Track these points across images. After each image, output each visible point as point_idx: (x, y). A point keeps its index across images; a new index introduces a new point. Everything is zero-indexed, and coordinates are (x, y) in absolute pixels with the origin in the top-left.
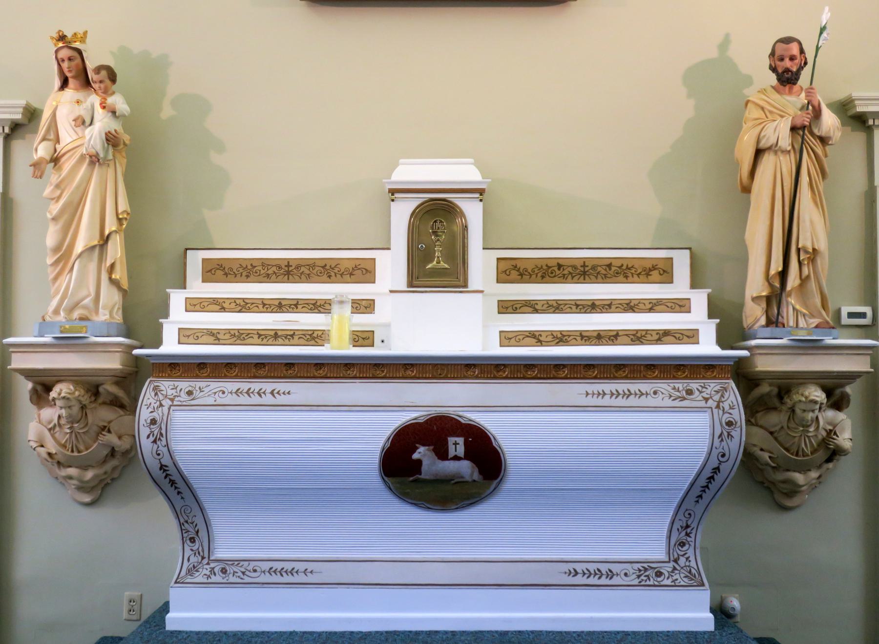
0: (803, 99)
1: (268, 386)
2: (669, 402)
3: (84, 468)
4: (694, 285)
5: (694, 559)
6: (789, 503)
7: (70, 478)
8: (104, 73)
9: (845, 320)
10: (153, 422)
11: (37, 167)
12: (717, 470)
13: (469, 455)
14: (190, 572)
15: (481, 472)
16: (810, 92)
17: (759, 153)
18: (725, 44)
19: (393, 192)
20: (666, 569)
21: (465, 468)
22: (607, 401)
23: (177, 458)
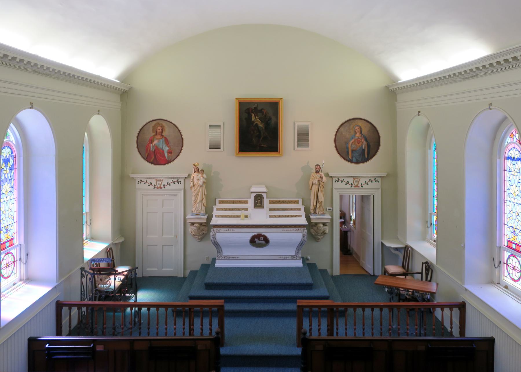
1: (231, 229)
2: (295, 232)
6: (318, 241)
8: (202, 171)
9: (328, 210)
10: (213, 235)
11: (191, 188)
12: (303, 242)
13: (264, 240)
14: (219, 258)
15: (266, 242)
18: (308, 162)
19: (251, 193)
20: (295, 256)
21: (263, 242)
22: (286, 231)
23: (217, 241)
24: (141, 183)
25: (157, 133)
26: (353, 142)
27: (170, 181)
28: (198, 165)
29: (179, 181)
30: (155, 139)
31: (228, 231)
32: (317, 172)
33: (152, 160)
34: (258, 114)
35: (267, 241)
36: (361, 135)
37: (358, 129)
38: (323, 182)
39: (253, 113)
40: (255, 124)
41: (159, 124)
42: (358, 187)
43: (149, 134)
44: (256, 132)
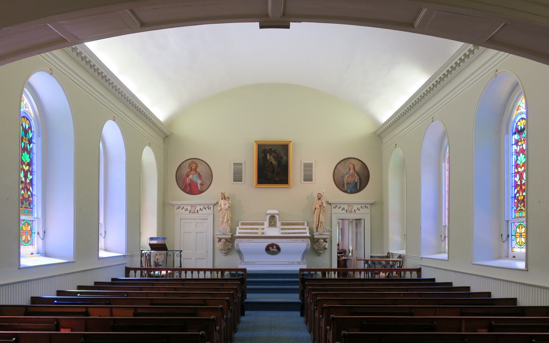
0: (321, 202)
1: (251, 240)
2: (301, 242)
3: (225, 251)
4: (307, 226)
5: (305, 261)
6: (320, 255)
7: (223, 252)
8: (228, 198)
9: (328, 231)
12: (307, 250)
16: (322, 201)
17: (315, 209)
18: (312, 193)
21: (276, 250)
24: (179, 209)
25: (192, 169)
26: (348, 177)
27: (202, 207)
28: (224, 193)
29: (209, 207)
30: (190, 174)
31: (248, 241)
32: (319, 199)
33: (188, 191)
34: (273, 154)
35: (278, 249)
36: (354, 171)
37: (352, 166)
38: (324, 207)
39: (268, 153)
40: (270, 161)
41: (193, 162)
42: (352, 212)
43: (186, 170)
44: (270, 168)
